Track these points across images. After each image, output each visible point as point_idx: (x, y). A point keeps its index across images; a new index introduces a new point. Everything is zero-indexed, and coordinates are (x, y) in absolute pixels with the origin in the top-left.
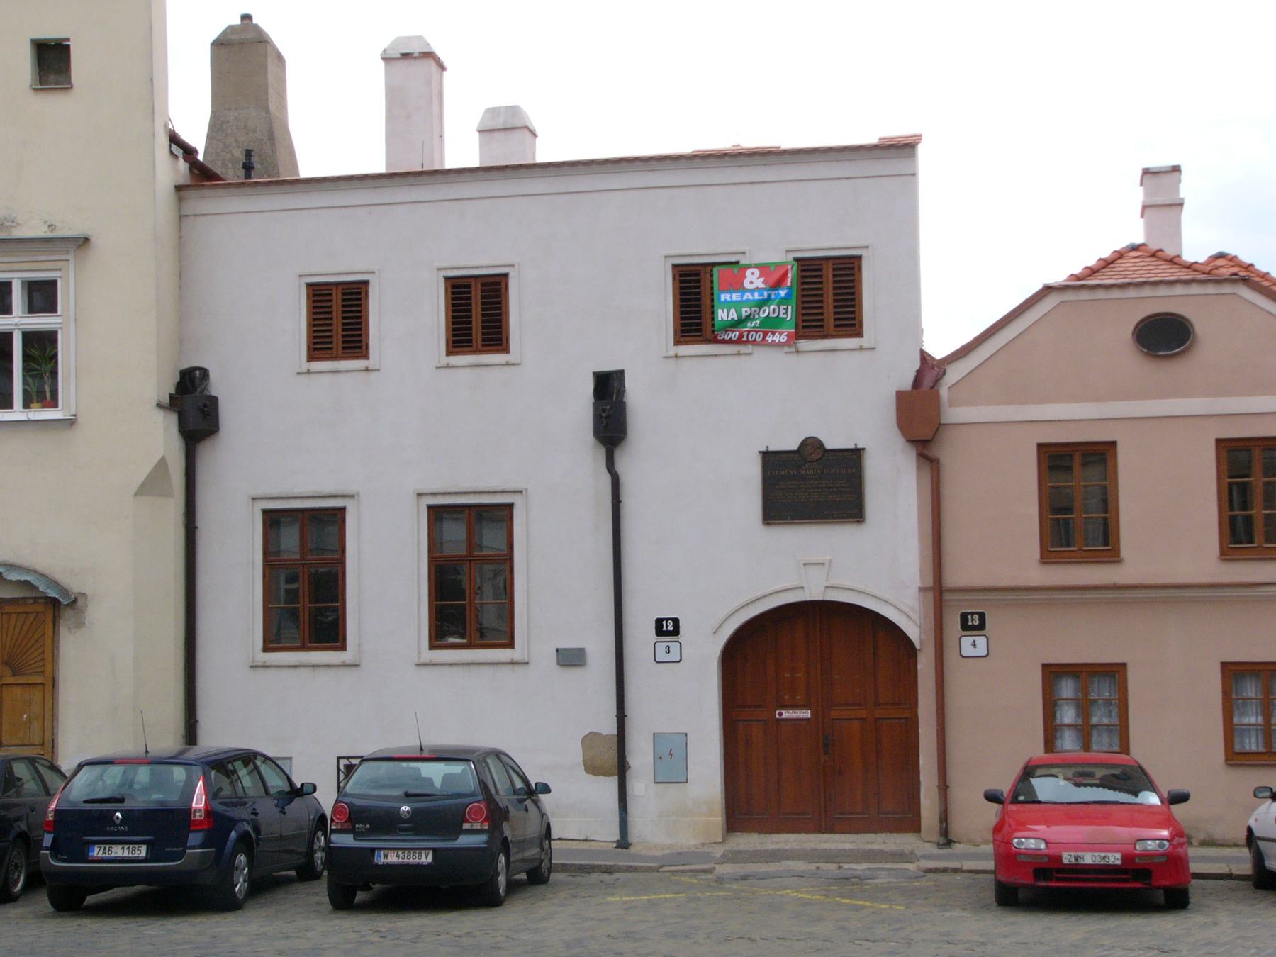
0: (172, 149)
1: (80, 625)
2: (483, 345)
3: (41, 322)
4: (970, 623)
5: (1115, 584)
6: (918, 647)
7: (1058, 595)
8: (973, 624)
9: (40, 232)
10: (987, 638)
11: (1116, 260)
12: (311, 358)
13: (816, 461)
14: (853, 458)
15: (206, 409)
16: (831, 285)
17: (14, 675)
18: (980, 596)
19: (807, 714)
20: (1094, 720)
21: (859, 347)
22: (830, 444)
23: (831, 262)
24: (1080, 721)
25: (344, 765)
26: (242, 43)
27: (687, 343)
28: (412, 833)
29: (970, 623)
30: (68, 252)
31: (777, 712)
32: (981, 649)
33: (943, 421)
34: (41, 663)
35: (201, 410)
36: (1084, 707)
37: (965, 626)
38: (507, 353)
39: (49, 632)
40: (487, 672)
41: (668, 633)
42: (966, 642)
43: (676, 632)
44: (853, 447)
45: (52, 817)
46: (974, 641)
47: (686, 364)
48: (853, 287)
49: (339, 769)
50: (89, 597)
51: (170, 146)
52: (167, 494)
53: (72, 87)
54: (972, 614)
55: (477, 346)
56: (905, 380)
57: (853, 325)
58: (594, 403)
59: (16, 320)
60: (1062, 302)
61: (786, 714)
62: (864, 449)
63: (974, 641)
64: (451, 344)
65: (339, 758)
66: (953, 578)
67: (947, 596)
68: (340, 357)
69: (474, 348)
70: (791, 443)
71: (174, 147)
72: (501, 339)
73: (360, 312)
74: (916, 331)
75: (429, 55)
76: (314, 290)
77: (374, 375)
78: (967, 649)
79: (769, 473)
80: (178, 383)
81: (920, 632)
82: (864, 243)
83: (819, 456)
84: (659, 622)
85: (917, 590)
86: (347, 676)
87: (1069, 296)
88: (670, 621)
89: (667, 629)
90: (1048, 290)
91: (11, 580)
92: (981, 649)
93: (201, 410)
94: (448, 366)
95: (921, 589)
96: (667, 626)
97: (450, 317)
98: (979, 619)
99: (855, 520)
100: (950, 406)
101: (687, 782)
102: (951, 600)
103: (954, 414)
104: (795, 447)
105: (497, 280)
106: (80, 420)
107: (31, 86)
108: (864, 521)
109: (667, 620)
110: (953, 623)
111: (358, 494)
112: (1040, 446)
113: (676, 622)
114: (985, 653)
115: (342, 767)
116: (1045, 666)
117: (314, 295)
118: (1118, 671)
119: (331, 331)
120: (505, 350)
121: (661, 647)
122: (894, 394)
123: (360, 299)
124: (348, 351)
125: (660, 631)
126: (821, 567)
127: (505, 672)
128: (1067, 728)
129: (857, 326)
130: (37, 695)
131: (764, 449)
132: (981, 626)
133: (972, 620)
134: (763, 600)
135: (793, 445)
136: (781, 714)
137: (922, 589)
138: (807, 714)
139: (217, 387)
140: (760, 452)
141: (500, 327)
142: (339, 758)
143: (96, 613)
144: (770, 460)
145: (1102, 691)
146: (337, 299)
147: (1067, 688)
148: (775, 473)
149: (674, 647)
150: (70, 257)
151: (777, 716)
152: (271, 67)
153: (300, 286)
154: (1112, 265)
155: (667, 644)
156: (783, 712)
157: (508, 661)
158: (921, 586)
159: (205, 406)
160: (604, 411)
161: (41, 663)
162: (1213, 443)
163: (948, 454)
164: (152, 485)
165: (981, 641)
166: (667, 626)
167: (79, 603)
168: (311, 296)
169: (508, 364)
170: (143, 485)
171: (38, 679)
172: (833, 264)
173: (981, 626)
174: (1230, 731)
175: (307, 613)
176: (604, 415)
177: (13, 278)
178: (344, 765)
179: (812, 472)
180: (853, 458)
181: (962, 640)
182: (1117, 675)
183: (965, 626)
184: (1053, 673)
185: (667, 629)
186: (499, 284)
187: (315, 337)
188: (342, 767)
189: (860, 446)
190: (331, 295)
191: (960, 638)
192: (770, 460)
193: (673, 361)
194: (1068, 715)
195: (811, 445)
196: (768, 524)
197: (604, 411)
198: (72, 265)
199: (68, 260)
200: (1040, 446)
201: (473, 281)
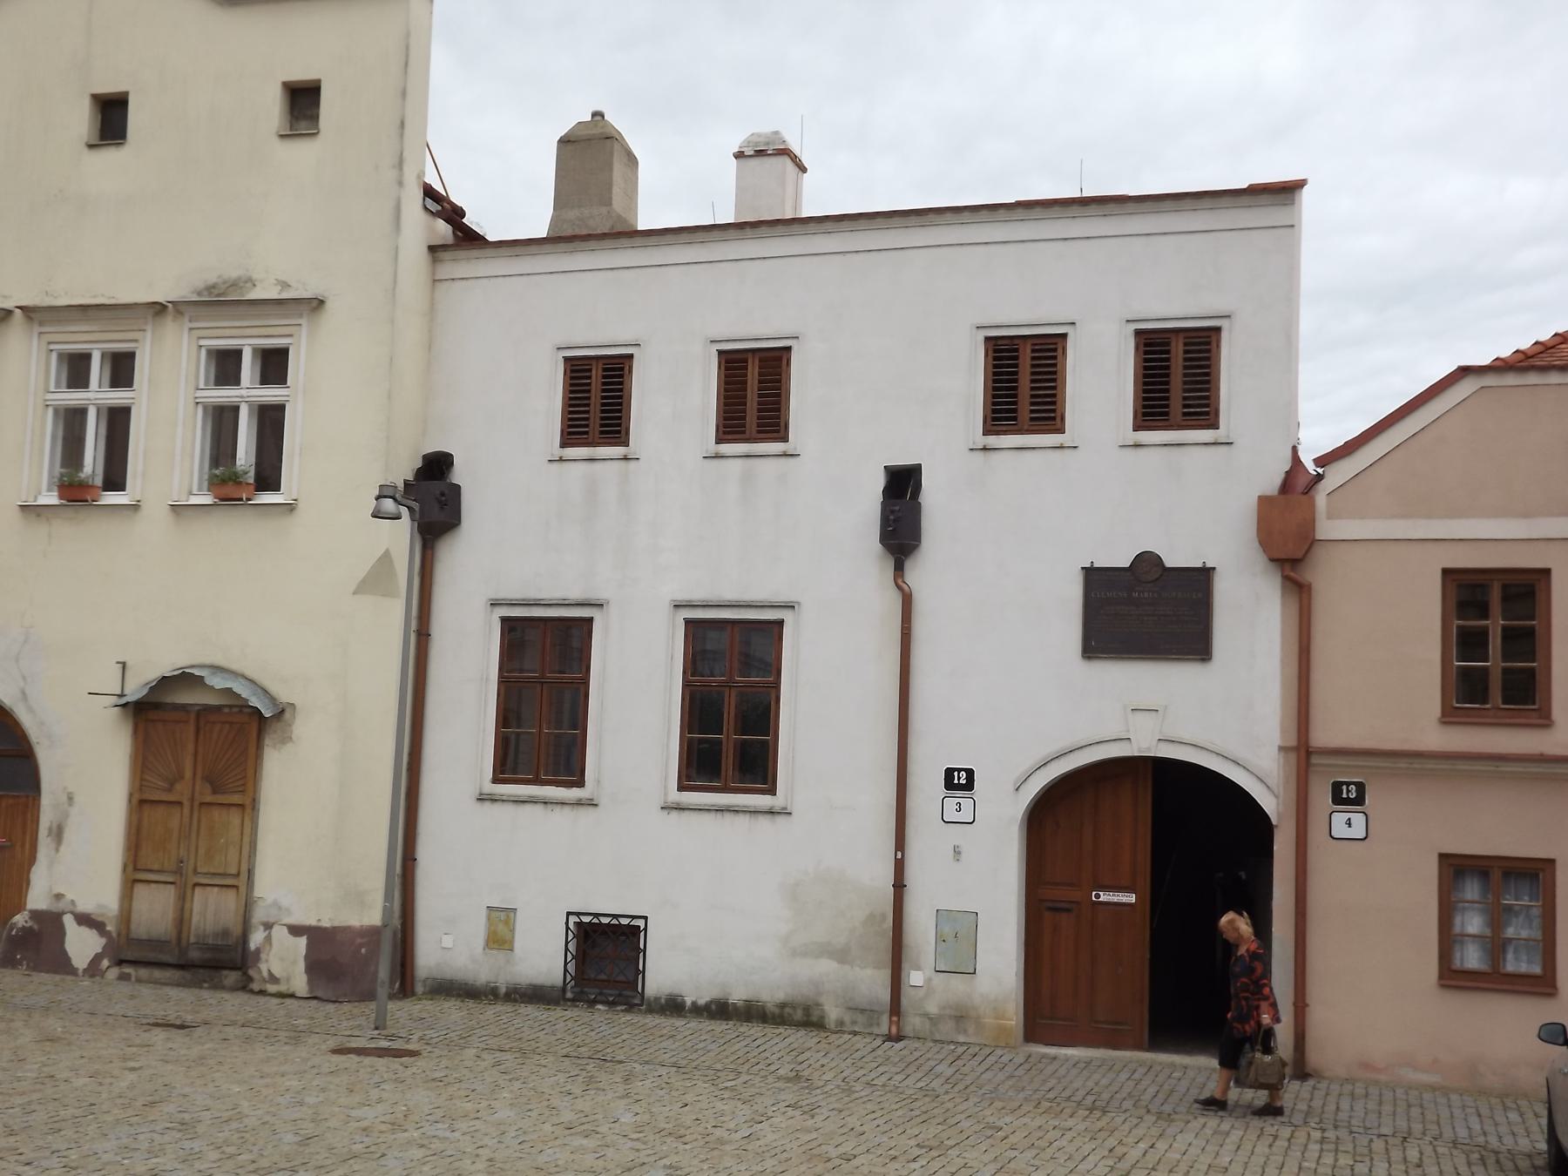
0: (426, 203)
1: (286, 739)
2: (759, 432)
3: (271, 394)
4: (1345, 796)
5: (1542, 755)
6: (1274, 822)
7: (1462, 766)
8: (1348, 797)
9: (273, 293)
11: (1558, 345)
13: (1152, 582)
14: (1199, 580)
15: (443, 498)
16: (1180, 362)
17: (215, 792)
18: (1360, 762)
19: (1131, 898)
20: (1510, 932)
22: (1170, 563)
23: (1181, 335)
24: (1488, 932)
25: (575, 922)
26: (589, 140)
27: (998, 433)
28: (623, 1008)
29: (1345, 796)
30: (301, 316)
31: (1094, 893)
32: (1358, 831)
33: (1318, 537)
34: (241, 782)
35: (437, 498)
36: (1497, 917)
37: (1338, 799)
38: (1203, 660)
39: (252, 750)
40: (743, 820)
41: (960, 787)
42: (1339, 819)
43: (969, 786)
44: (1200, 565)
45: (1529, 962)
46: (1349, 819)
47: (995, 457)
48: (1208, 367)
49: (568, 928)
50: (297, 708)
51: (424, 200)
52: (389, 593)
53: (318, 133)
54: (1348, 784)
55: (751, 433)
56: (1271, 481)
57: (1207, 413)
58: (882, 503)
59: (244, 392)
60: (1482, 387)
62: (1214, 568)
64: (721, 429)
65: (569, 914)
66: (1322, 736)
69: (747, 436)
70: (1122, 558)
71: (429, 202)
72: (778, 425)
73: (621, 390)
74: (1290, 420)
75: (785, 152)
76: (572, 365)
77: (632, 464)
78: (1340, 829)
79: (1093, 595)
80: (419, 470)
81: (1278, 804)
82: (1223, 309)
83: (1157, 576)
84: (949, 773)
85: (1277, 748)
86: (586, 814)
87: (1490, 380)
89: (959, 782)
90: (1464, 372)
91: (212, 687)
92: (1358, 831)
93: (437, 498)
94: (718, 456)
95: (1281, 749)
96: (959, 778)
97: (722, 404)
98: (1356, 791)
99: (1199, 657)
100: (1330, 517)
101: (975, 973)
103: (1326, 529)
105: (777, 354)
106: (301, 505)
107: (278, 132)
108: (1210, 659)
109: (959, 770)
110: (1321, 797)
112: (1446, 572)
113: (970, 773)
114: (1362, 835)
115: (571, 926)
117: (572, 371)
118: (1543, 870)
119: (588, 412)
120: (782, 438)
121: (951, 804)
122: (1254, 502)
123: (621, 376)
125: (950, 784)
126: (1154, 713)
127: (764, 822)
128: (1471, 939)
129: (1212, 415)
130: (234, 818)
132: (1359, 800)
135: (1124, 561)
136: (1098, 896)
137: (1283, 749)
138: (1131, 898)
140: (1082, 568)
141: (779, 410)
142: (569, 914)
143: (304, 728)
144: (1093, 576)
145: (1519, 898)
147: (1471, 890)
148: (1100, 594)
149: (967, 804)
150: (303, 321)
151: (1094, 899)
152: (618, 169)
153: (557, 362)
154: (1553, 350)
156: (1101, 893)
157: (766, 809)
158: (1281, 745)
159: (443, 494)
160: (893, 512)
161: (241, 782)
163: (1324, 575)
164: (375, 581)
165: (1358, 820)
166: (959, 778)
167: (287, 715)
168: (568, 372)
169: (785, 455)
170: (363, 581)
171: (236, 799)
172: (1185, 338)
173: (1359, 800)
174: (1448, 940)
175: (723, 773)
176: (892, 517)
177: (244, 345)
178: (575, 922)
179: (1146, 595)
180: (1199, 580)
181: (1332, 816)
182: (1541, 876)
183: (1338, 799)
184: (1455, 868)
185: (959, 782)
186: (780, 359)
187: (570, 419)
188: (571, 926)
189: (1209, 565)
190: (590, 370)
191: (1331, 814)
192: (1093, 576)
193: (981, 454)
194: (1473, 923)
195: (1147, 562)
196: (1089, 658)
197: (893, 512)
198: (304, 330)
199: (300, 325)
200: (1446, 572)
201: (750, 356)
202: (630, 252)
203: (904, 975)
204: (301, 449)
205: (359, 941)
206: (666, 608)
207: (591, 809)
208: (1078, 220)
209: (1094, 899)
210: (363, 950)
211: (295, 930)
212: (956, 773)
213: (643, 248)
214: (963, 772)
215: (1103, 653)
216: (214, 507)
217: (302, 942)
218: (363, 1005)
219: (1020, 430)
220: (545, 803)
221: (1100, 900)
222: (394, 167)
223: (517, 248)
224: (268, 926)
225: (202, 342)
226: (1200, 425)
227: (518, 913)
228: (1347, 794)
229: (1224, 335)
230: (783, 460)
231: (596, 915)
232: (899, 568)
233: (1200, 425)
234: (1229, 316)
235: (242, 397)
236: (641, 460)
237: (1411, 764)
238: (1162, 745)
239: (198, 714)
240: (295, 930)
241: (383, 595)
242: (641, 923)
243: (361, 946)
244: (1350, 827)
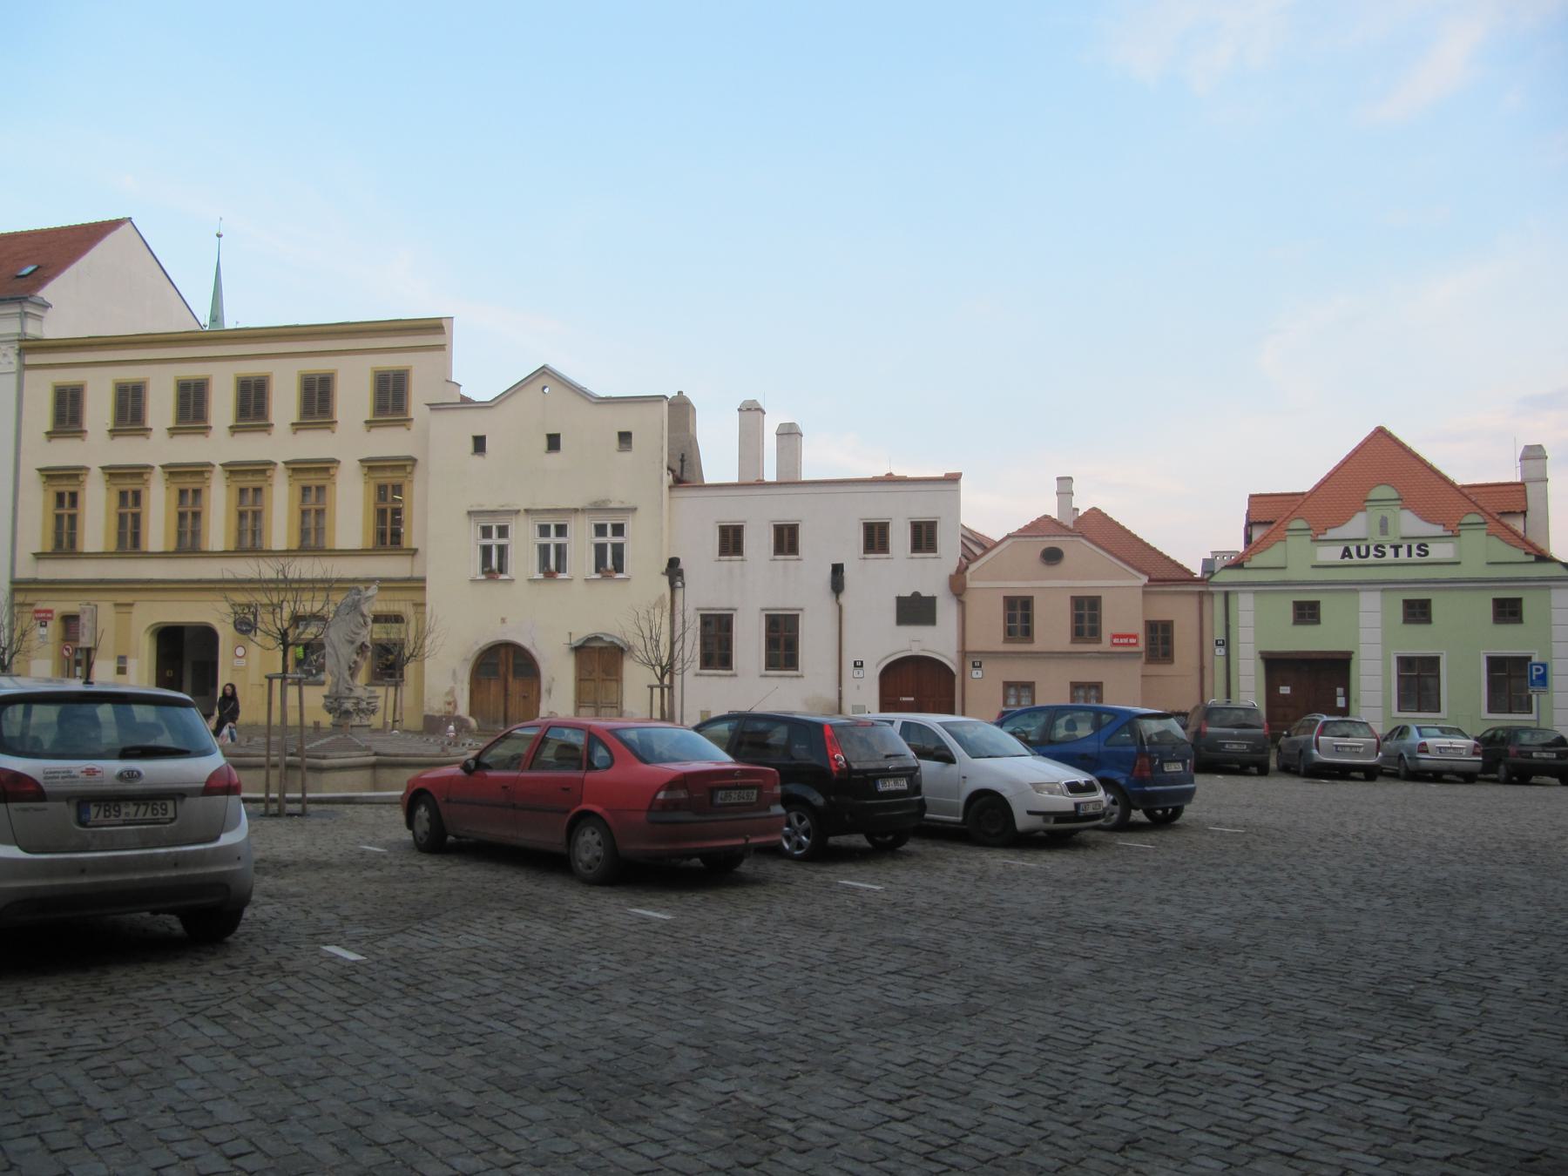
12: (720, 555)
19: (912, 699)
22: (923, 594)
37: (974, 666)
40: (787, 680)
61: (904, 699)
70: (908, 594)
110: (969, 665)
127: (795, 680)
138: (912, 699)
139: (682, 565)
146: (786, 532)
165: (980, 672)
183: (974, 666)
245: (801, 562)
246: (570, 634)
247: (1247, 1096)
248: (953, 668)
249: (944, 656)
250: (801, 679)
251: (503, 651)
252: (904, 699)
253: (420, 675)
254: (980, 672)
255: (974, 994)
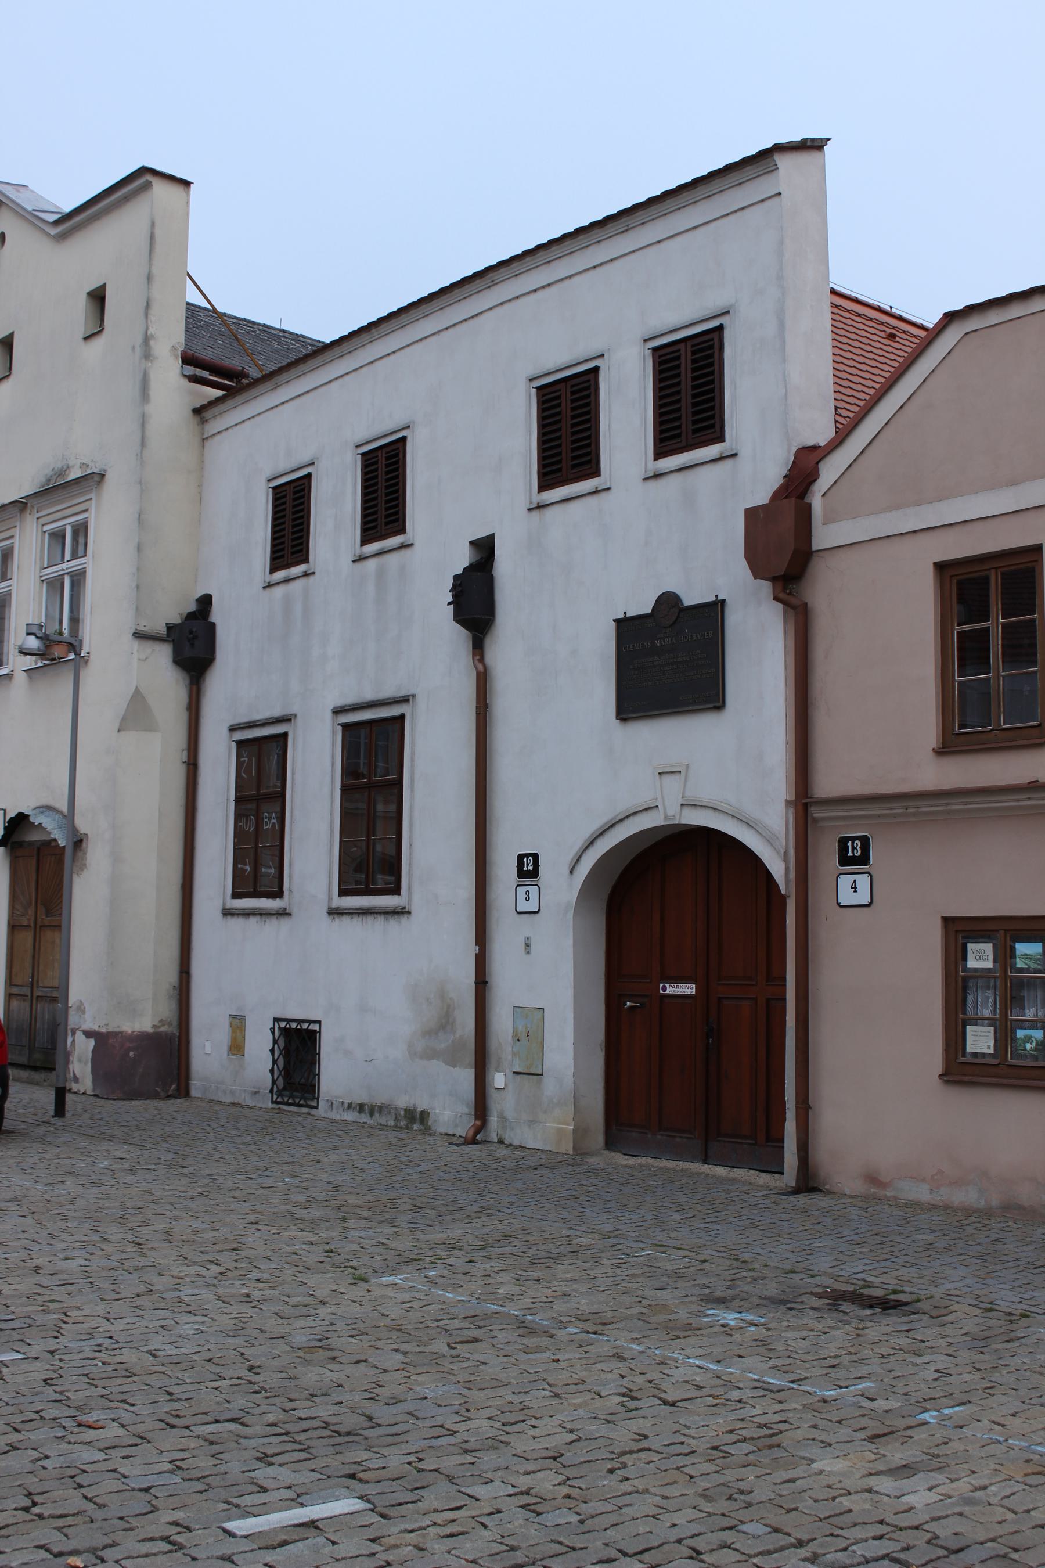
4: (850, 854)
10: (871, 876)
19: (690, 990)
21: (536, 505)
22: (689, 599)
31: (661, 985)
37: (845, 860)
42: (845, 881)
44: (714, 599)
46: (855, 881)
47: (549, 512)
60: (967, 333)
61: (672, 989)
63: (855, 881)
67: (817, 813)
68: (571, 479)
70: (643, 605)
78: (846, 896)
88: (530, 858)
92: (863, 897)
94: (657, 476)
99: (711, 705)
102: (824, 819)
104: (648, 610)
110: (827, 856)
111: (295, 716)
112: (941, 567)
114: (866, 900)
116: (947, 921)
124: (550, 477)
125: (522, 874)
131: (621, 616)
132: (864, 859)
133: (853, 848)
134: (627, 822)
137: (788, 803)
138: (690, 990)
139: (216, 615)
150: (92, 495)
151: (661, 992)
155: (528, 888)
156: (667, 985)
162: (930, 571)
165: (863, 881)
170: (124, 719)
183: (845, 860)
192: (626, 627)
200: (941, 567)
202: (649, 227)
203: (488, 1078)
204: (91, 608)
205: (128, 1044)
206: (329, 714)
207: (286, 918)
208: (603, 243)
209: (661, 992)
210: (132, 1054)
211: (88, 1034)
212: (525, 860)
213: (738, 187)
214: (857, 841)
215: (634, 712)
216: (44, 669)
217: (92, 1042)
218: (127, 1104)
219: (684, 447)
220: (261, 914)
221: (667, 992)
222: (152, 336)
223: (434, 302)
224: (74, 1033)
225: (46, 528)
226: (708, 441)
227: (936, 1061)
228: (853, 852)
229: (727, 334)
230: (403, 552)
231: (300, 1021)
232: (478, 647)
233: (708, 441)
234: (728, 312)
235: (63, 570)
236: (613, 491)
237: (947, 805)
238: (687, 811)
239: (39, 849)
240: (88, 1034)
241: (146, 730)
242: (316, 1027)
243: (130, 1049)
244: (855, 891)
245: (312, 578)
246: (603, 355)
247: (416, 1492)
248: (777, 868)
249: (748, 824)
250: (404, 919)
251: (392, 879)
252: (672, 989)
253: (789, 451)
254: (863, 881)
255: (253, 1405)
